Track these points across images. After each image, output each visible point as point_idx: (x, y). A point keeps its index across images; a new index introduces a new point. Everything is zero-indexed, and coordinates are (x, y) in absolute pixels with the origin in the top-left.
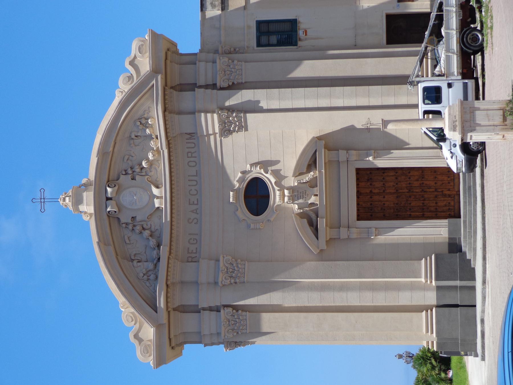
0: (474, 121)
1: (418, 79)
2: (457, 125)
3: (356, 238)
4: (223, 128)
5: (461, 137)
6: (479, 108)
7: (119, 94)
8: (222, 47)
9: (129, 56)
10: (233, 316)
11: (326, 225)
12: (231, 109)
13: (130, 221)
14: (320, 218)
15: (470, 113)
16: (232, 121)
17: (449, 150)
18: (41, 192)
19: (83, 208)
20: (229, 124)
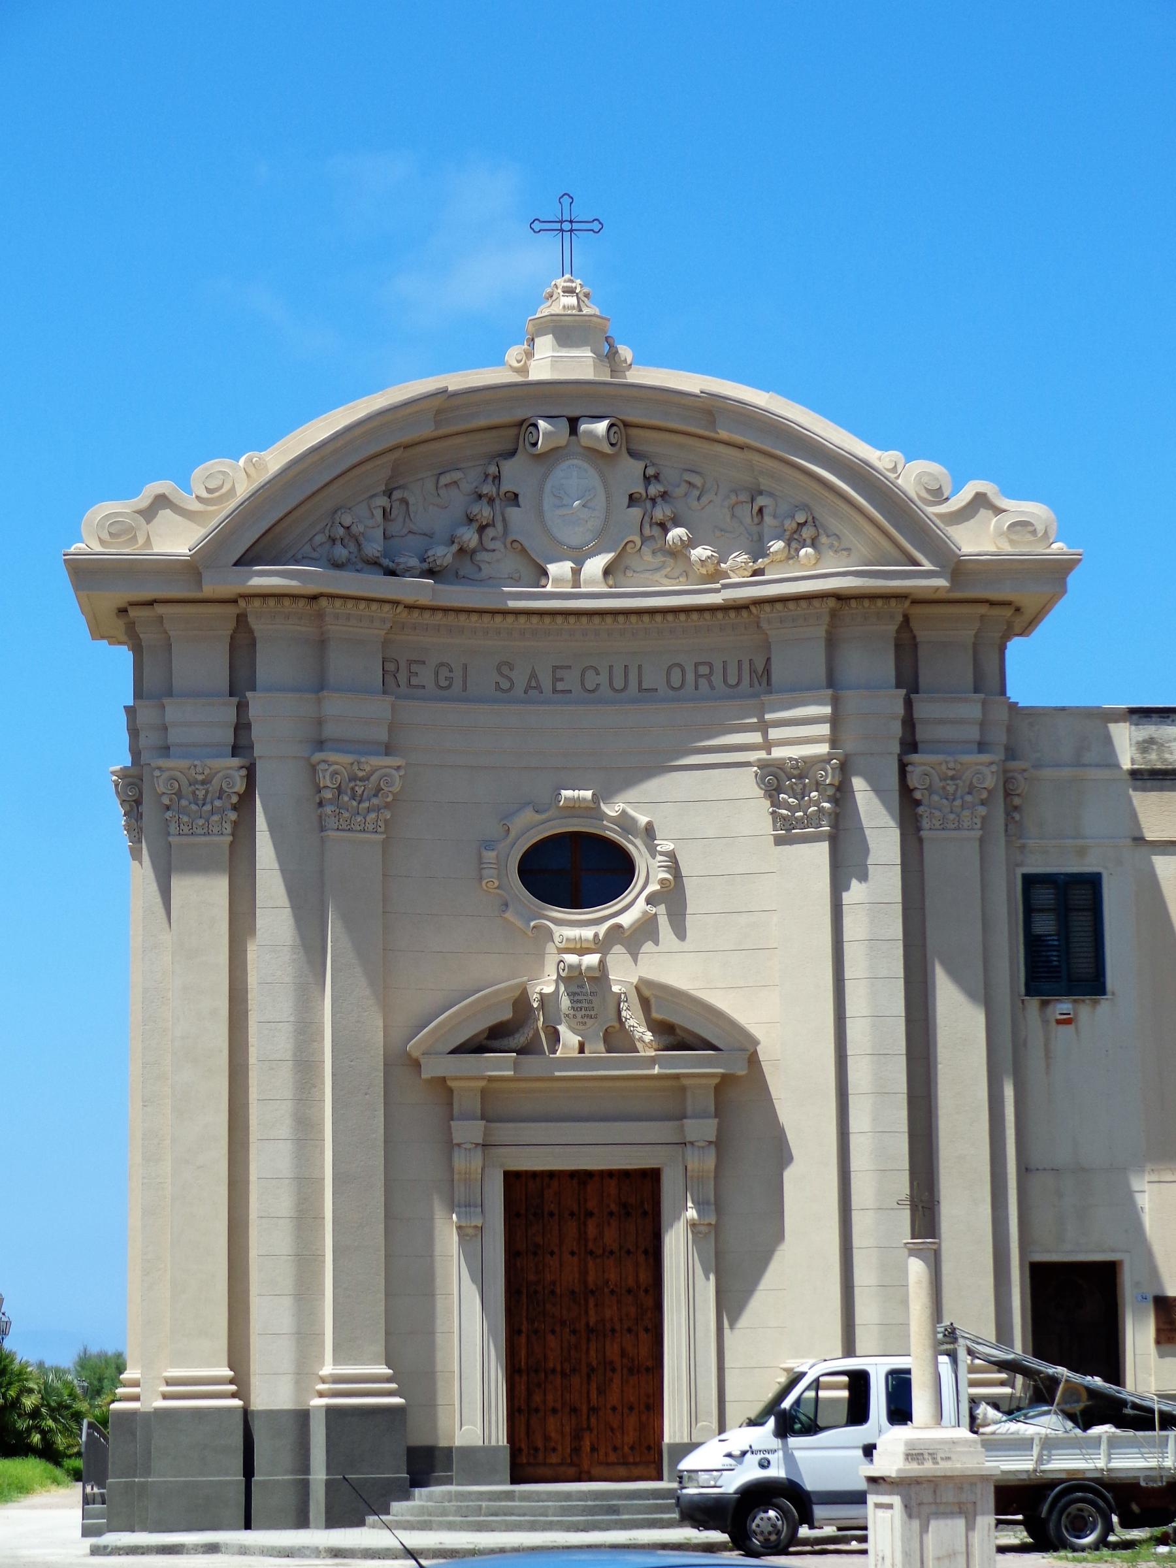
0: (936, 1514)
1: (962, 1354)
2: (923, 1464)
3: (451, 1169)
4: (784, 772)
5: (889, 1477)
6: (973, 1529)
7: (887, 460)
8: (1025, 770)
9: (1000, 490)
10: (221, 794)
11: (491, 1079)
12: (842, 795)
13: (505, 487)
14: (516, 1059)
15: (960, 1504)
16: (806, 798)
17: (751, 1447)
18: (593, 221)
19: (545, 345)
20: (798, 789)
